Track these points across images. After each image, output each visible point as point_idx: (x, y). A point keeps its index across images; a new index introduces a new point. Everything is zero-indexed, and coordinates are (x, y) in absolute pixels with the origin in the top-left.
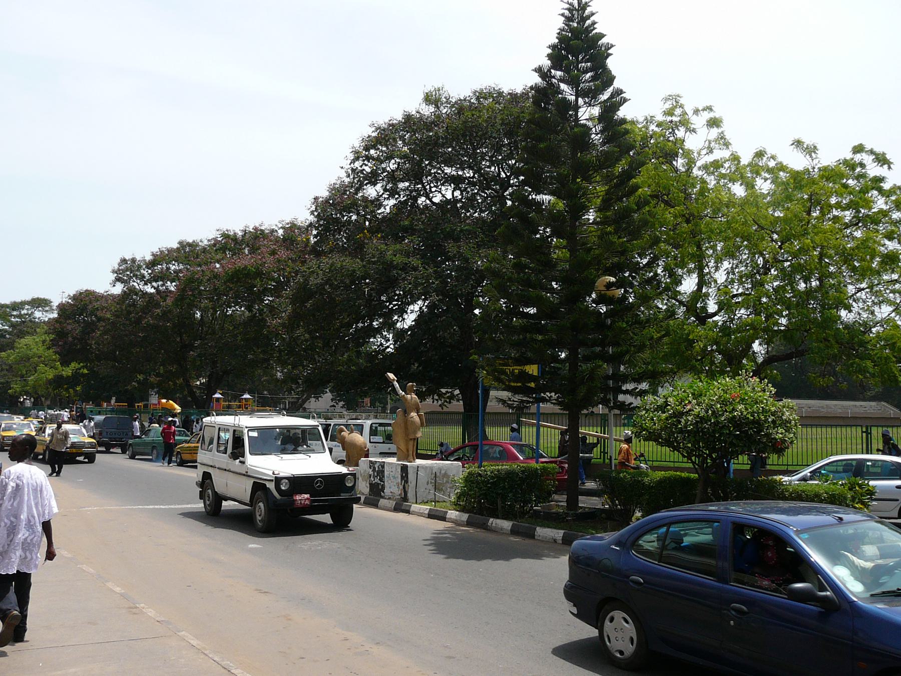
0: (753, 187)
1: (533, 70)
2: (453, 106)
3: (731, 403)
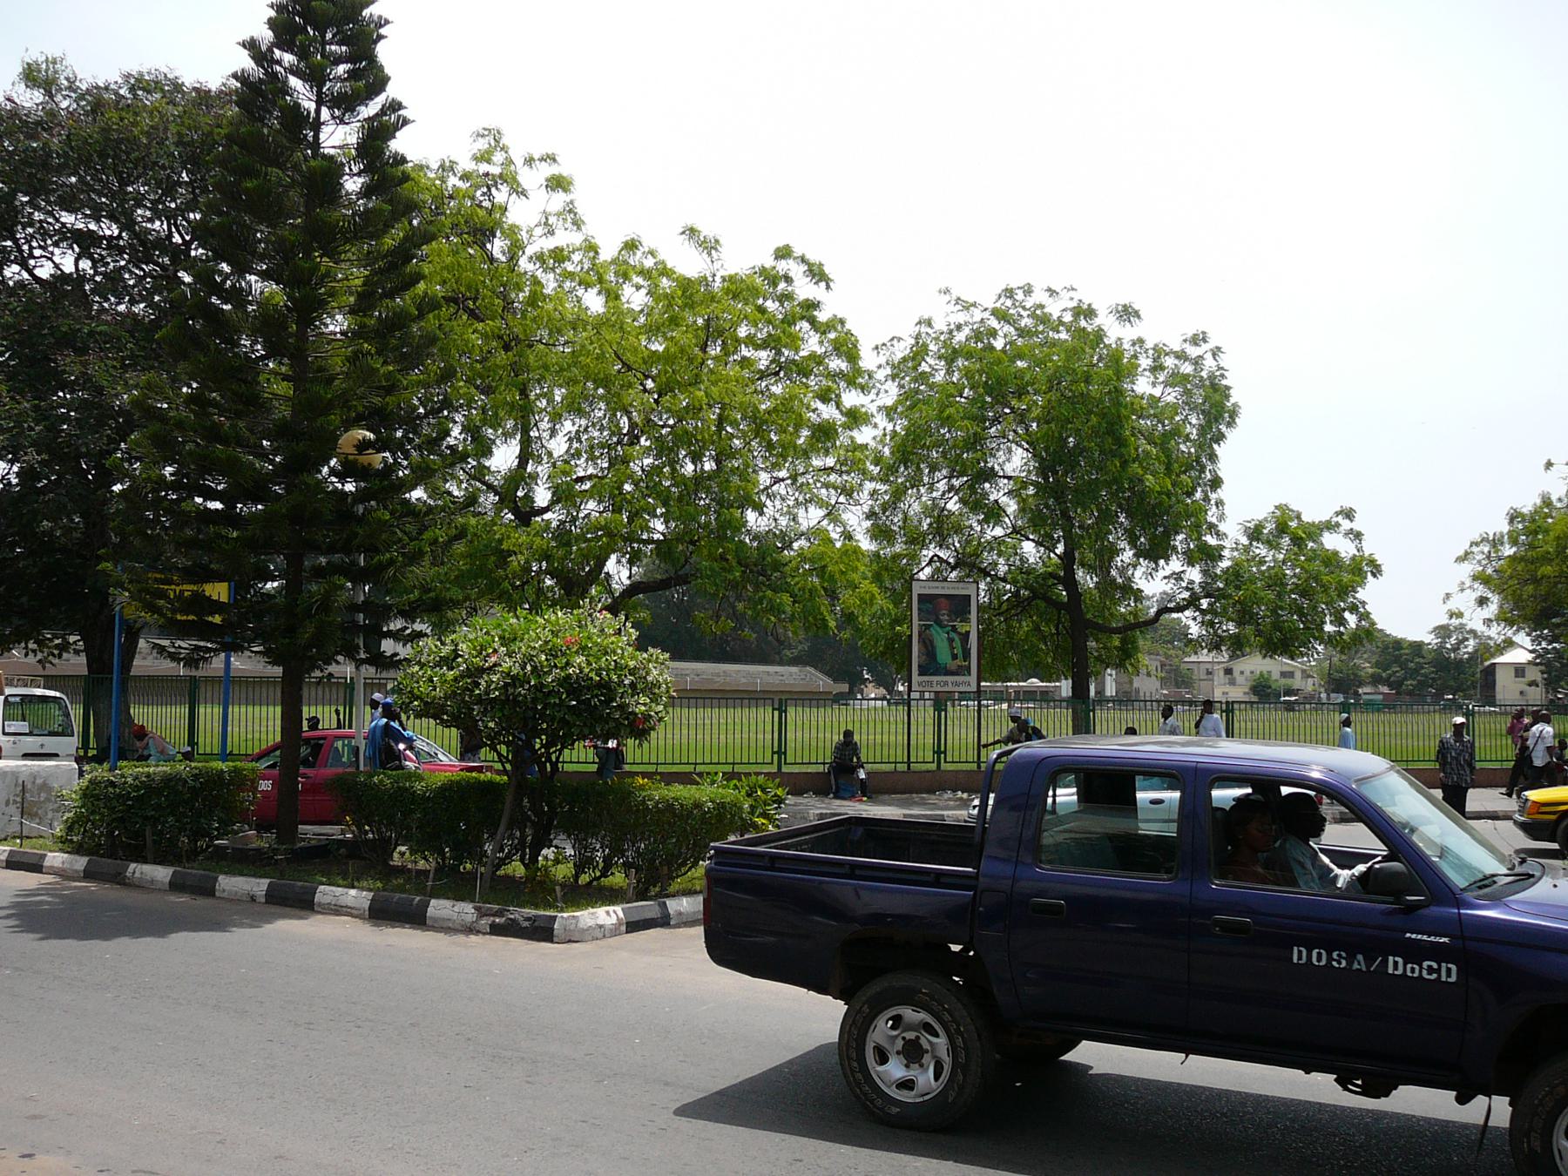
0: (617, 297)
1: (239, 43)
2: (82, 97)
3: (564, 654)
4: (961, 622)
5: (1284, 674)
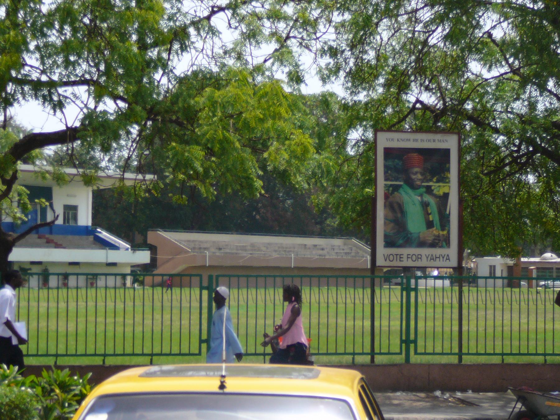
4: (438, 181)
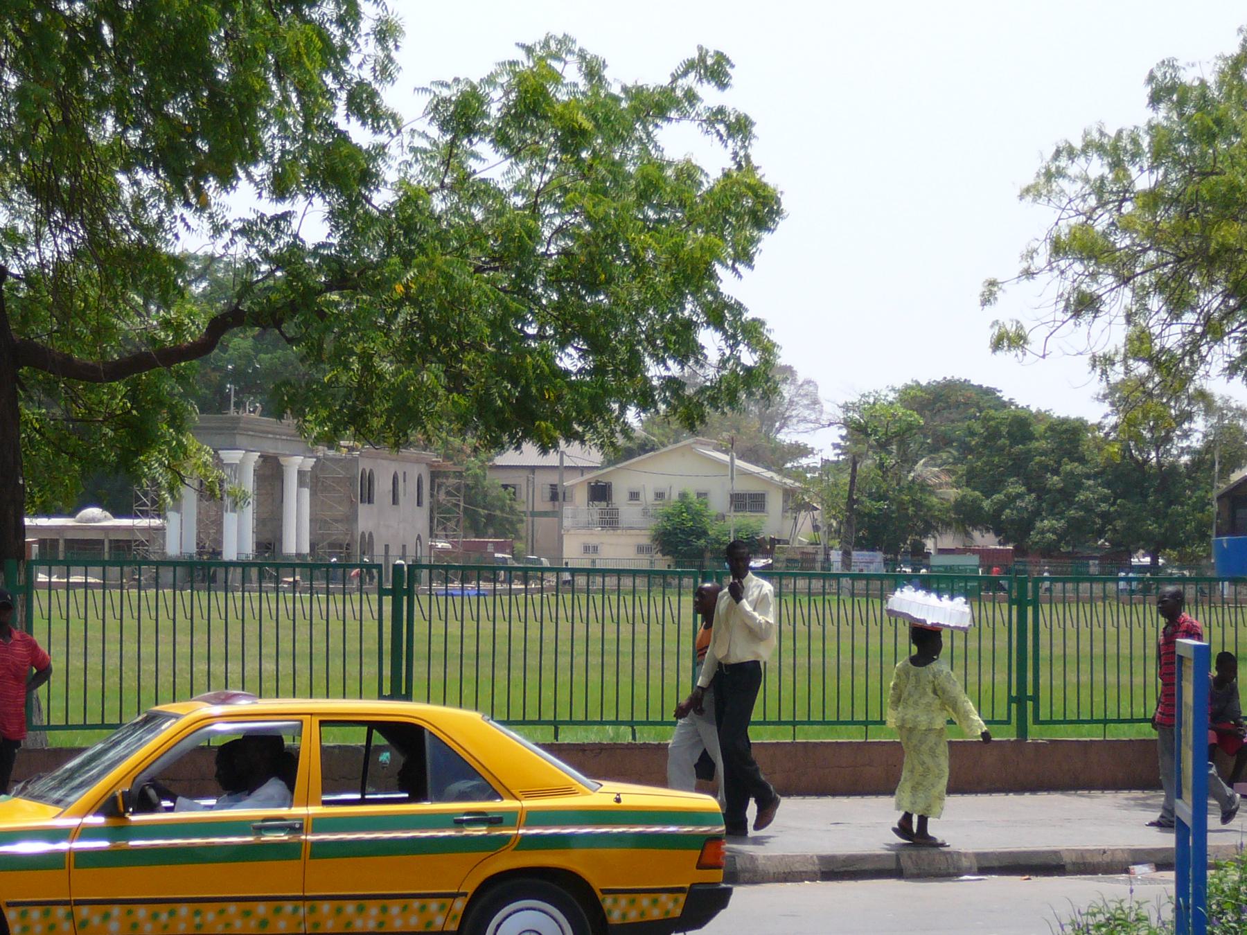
5: (741, 501)
